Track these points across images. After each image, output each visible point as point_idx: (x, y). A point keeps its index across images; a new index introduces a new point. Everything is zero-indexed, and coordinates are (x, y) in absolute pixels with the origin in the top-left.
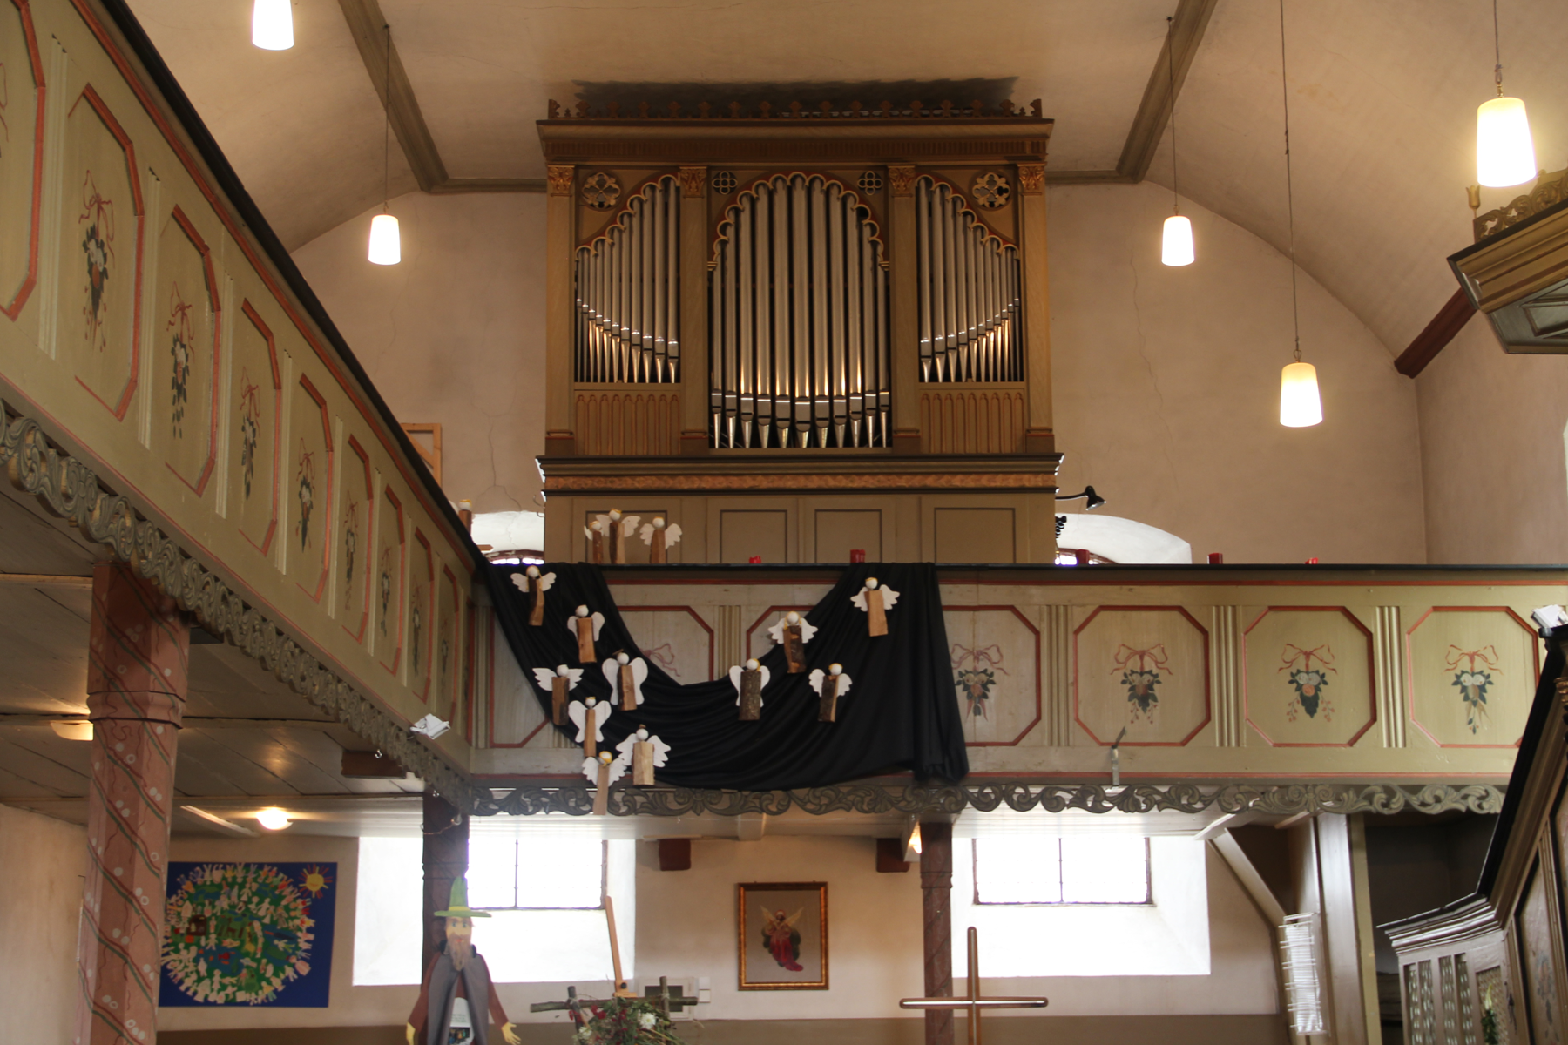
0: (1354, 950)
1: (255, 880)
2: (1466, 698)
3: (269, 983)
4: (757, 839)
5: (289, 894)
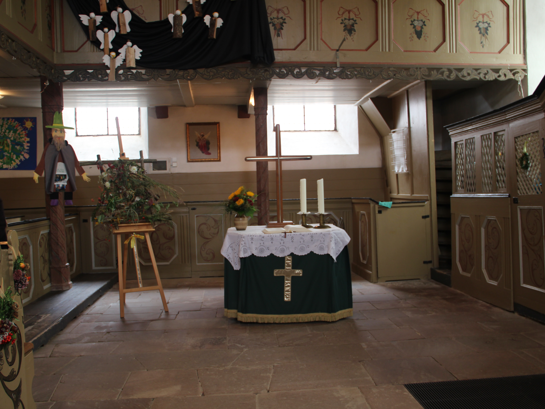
0: (426, 139)
1: (7, 124)
2: (480, 33)
3: (15, 161)
4: (193, 106)
5: (20, 129)
